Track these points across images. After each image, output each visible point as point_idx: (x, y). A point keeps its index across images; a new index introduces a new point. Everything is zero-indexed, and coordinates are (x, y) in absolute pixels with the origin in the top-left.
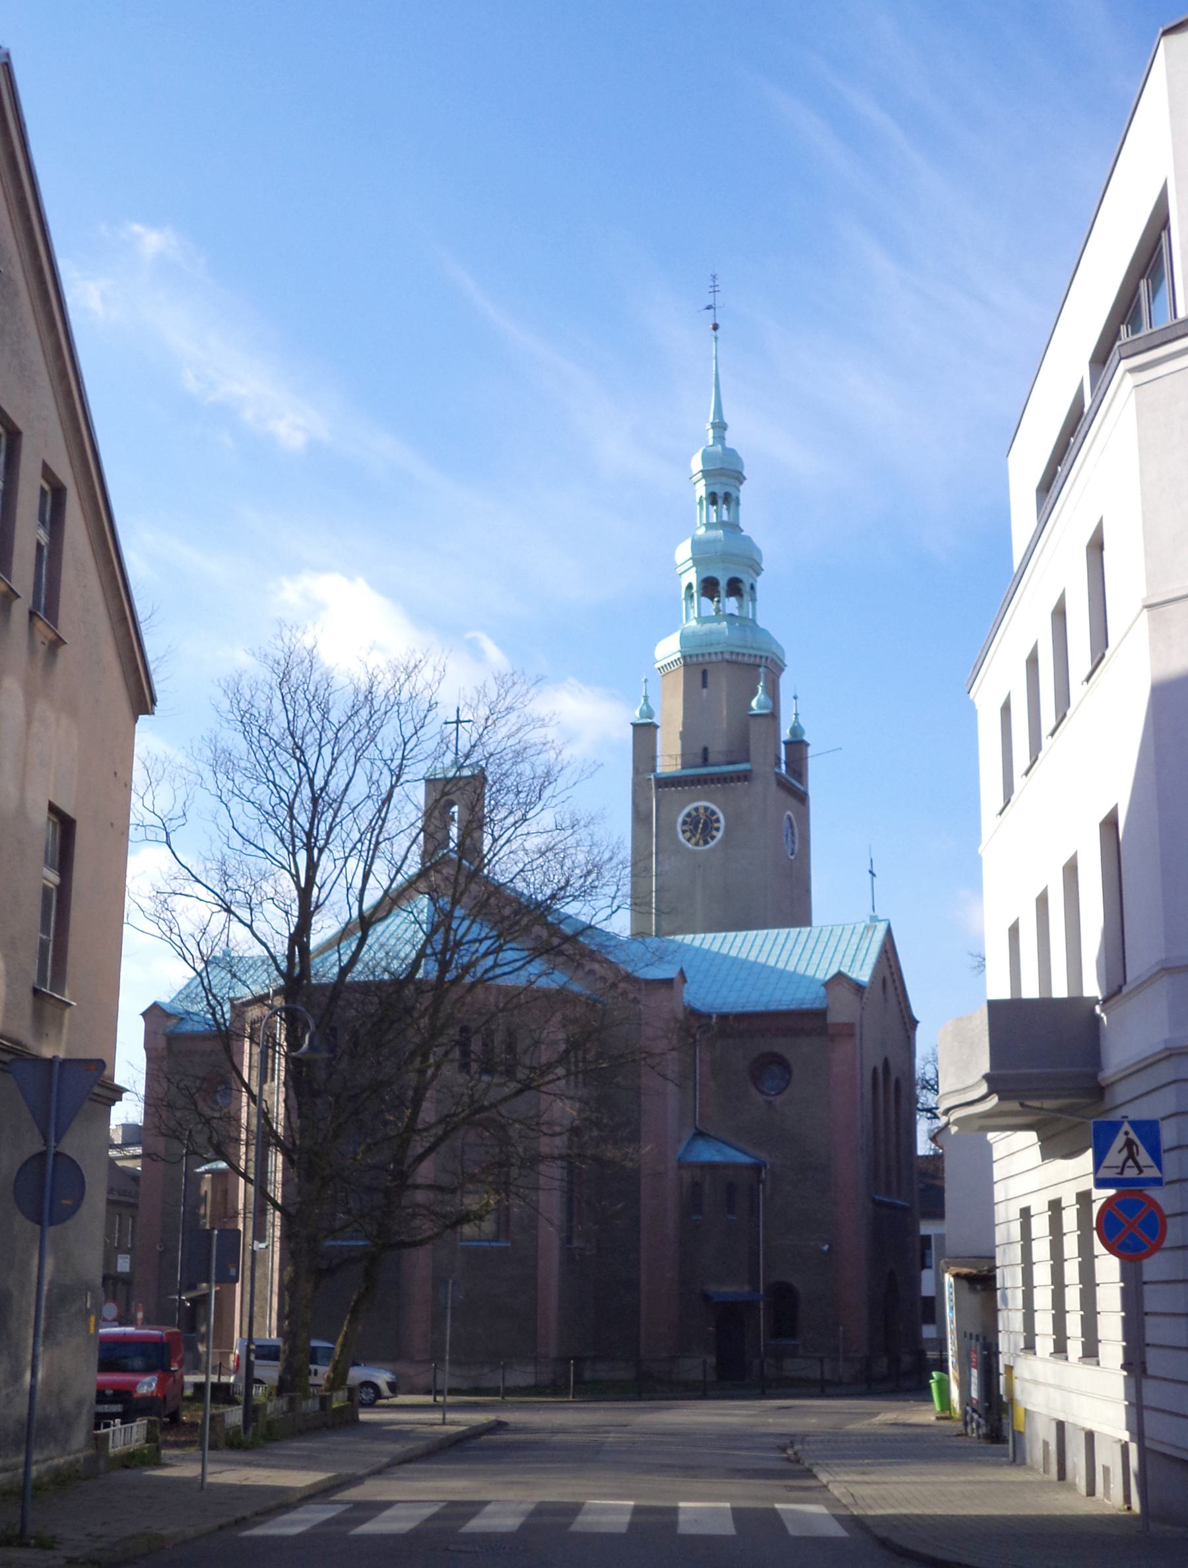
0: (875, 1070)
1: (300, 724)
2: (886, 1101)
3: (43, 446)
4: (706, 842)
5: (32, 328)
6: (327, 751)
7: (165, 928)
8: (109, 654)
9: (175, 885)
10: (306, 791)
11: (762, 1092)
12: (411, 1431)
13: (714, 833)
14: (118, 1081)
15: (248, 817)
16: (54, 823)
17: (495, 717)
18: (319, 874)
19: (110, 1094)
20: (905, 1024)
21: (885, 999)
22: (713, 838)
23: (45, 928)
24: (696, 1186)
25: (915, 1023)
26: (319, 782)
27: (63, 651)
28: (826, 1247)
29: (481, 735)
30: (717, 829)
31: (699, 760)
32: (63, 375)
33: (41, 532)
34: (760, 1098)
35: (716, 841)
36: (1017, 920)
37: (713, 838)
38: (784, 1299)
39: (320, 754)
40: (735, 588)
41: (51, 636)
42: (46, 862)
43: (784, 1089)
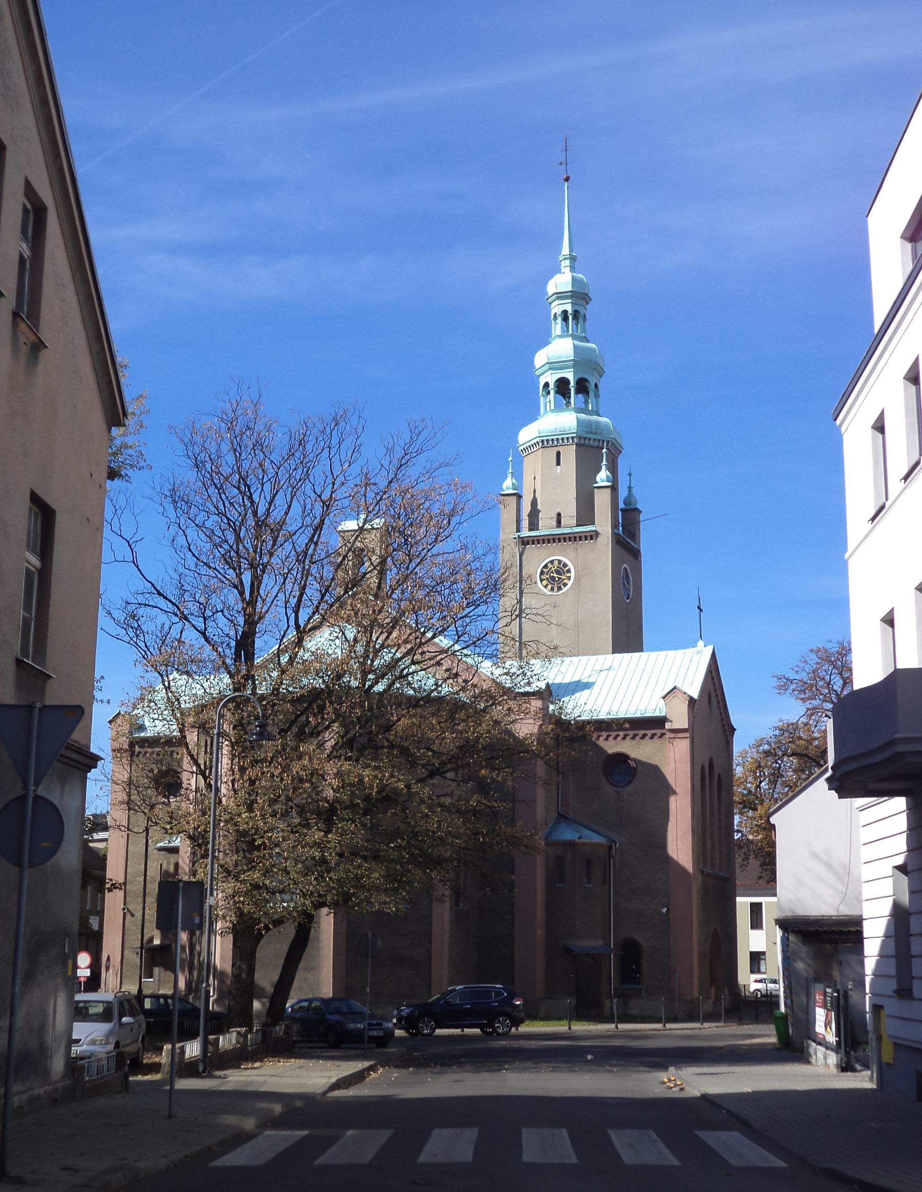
0: (703, 767)
1: (246, 465)
3: (27, 163)
4: (559, 589)
5: (15, 52)
6: (267, 487)
7: (132, 635)
8: (85, 365)
9: (141, 599)
10: (251, 522)
11: (612, 785)
14: (93, 749)
15: (202, 544)
16: (36, 514)
17: (408, 457)
18: (263, 586)
19: (86, 761)
21: (710, 710)
23: (27, 607)
24: (560, 860)
26: (261, 511)
27: (44, 354)
28: (664, 910)
29: (396, 475)
31: (554, 523)
32: (44, 102)
33: (24, 245)
34: (610, 789)
35: (567, 587)
36: (893, 609)
37: (565, 585)
38: (631, 954)
39: (262, 489)
41: (33, 338)
42: (28, 546)
43: (631, 781)
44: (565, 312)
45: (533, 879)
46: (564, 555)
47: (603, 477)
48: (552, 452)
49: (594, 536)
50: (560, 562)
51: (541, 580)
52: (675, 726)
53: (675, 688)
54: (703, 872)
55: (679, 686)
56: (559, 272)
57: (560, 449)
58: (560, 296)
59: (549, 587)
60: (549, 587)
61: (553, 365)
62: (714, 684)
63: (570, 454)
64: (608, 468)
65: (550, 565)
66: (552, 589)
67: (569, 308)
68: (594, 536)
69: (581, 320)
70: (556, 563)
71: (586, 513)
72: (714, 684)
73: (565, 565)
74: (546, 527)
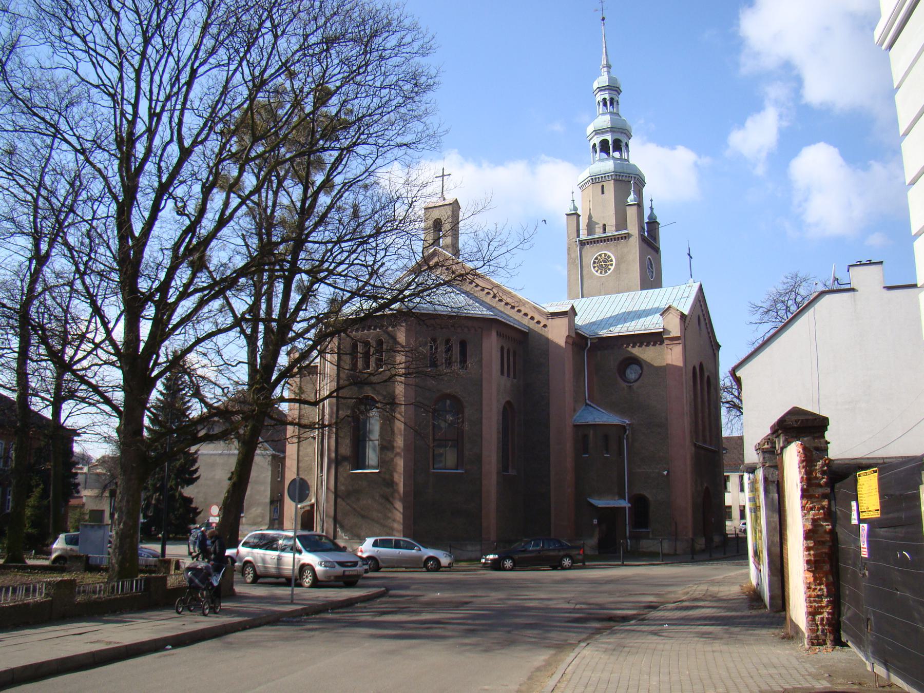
0: (694, 368)
2: (702, 389)
4: (606, 272)
25: (718, 346)
28: (665, 473)
38: (640, 505)
40: (618, 145)
44: (604, 99)
45: (562, 450)
47: (631, 199)
48: (599, 186)
49: (627, 237)
50: (606, 255)
52: (671, 335)
53: (670, 307)
55: (675, 305)
57: (604, 183)
58: (601, 89)
61: (597, 132)
63: (610, 187)
64: (635, 194)
67: (607, 97)
69: (615, 103)
71: (621, 222)
73: (609, 257)
74: (599, 234)
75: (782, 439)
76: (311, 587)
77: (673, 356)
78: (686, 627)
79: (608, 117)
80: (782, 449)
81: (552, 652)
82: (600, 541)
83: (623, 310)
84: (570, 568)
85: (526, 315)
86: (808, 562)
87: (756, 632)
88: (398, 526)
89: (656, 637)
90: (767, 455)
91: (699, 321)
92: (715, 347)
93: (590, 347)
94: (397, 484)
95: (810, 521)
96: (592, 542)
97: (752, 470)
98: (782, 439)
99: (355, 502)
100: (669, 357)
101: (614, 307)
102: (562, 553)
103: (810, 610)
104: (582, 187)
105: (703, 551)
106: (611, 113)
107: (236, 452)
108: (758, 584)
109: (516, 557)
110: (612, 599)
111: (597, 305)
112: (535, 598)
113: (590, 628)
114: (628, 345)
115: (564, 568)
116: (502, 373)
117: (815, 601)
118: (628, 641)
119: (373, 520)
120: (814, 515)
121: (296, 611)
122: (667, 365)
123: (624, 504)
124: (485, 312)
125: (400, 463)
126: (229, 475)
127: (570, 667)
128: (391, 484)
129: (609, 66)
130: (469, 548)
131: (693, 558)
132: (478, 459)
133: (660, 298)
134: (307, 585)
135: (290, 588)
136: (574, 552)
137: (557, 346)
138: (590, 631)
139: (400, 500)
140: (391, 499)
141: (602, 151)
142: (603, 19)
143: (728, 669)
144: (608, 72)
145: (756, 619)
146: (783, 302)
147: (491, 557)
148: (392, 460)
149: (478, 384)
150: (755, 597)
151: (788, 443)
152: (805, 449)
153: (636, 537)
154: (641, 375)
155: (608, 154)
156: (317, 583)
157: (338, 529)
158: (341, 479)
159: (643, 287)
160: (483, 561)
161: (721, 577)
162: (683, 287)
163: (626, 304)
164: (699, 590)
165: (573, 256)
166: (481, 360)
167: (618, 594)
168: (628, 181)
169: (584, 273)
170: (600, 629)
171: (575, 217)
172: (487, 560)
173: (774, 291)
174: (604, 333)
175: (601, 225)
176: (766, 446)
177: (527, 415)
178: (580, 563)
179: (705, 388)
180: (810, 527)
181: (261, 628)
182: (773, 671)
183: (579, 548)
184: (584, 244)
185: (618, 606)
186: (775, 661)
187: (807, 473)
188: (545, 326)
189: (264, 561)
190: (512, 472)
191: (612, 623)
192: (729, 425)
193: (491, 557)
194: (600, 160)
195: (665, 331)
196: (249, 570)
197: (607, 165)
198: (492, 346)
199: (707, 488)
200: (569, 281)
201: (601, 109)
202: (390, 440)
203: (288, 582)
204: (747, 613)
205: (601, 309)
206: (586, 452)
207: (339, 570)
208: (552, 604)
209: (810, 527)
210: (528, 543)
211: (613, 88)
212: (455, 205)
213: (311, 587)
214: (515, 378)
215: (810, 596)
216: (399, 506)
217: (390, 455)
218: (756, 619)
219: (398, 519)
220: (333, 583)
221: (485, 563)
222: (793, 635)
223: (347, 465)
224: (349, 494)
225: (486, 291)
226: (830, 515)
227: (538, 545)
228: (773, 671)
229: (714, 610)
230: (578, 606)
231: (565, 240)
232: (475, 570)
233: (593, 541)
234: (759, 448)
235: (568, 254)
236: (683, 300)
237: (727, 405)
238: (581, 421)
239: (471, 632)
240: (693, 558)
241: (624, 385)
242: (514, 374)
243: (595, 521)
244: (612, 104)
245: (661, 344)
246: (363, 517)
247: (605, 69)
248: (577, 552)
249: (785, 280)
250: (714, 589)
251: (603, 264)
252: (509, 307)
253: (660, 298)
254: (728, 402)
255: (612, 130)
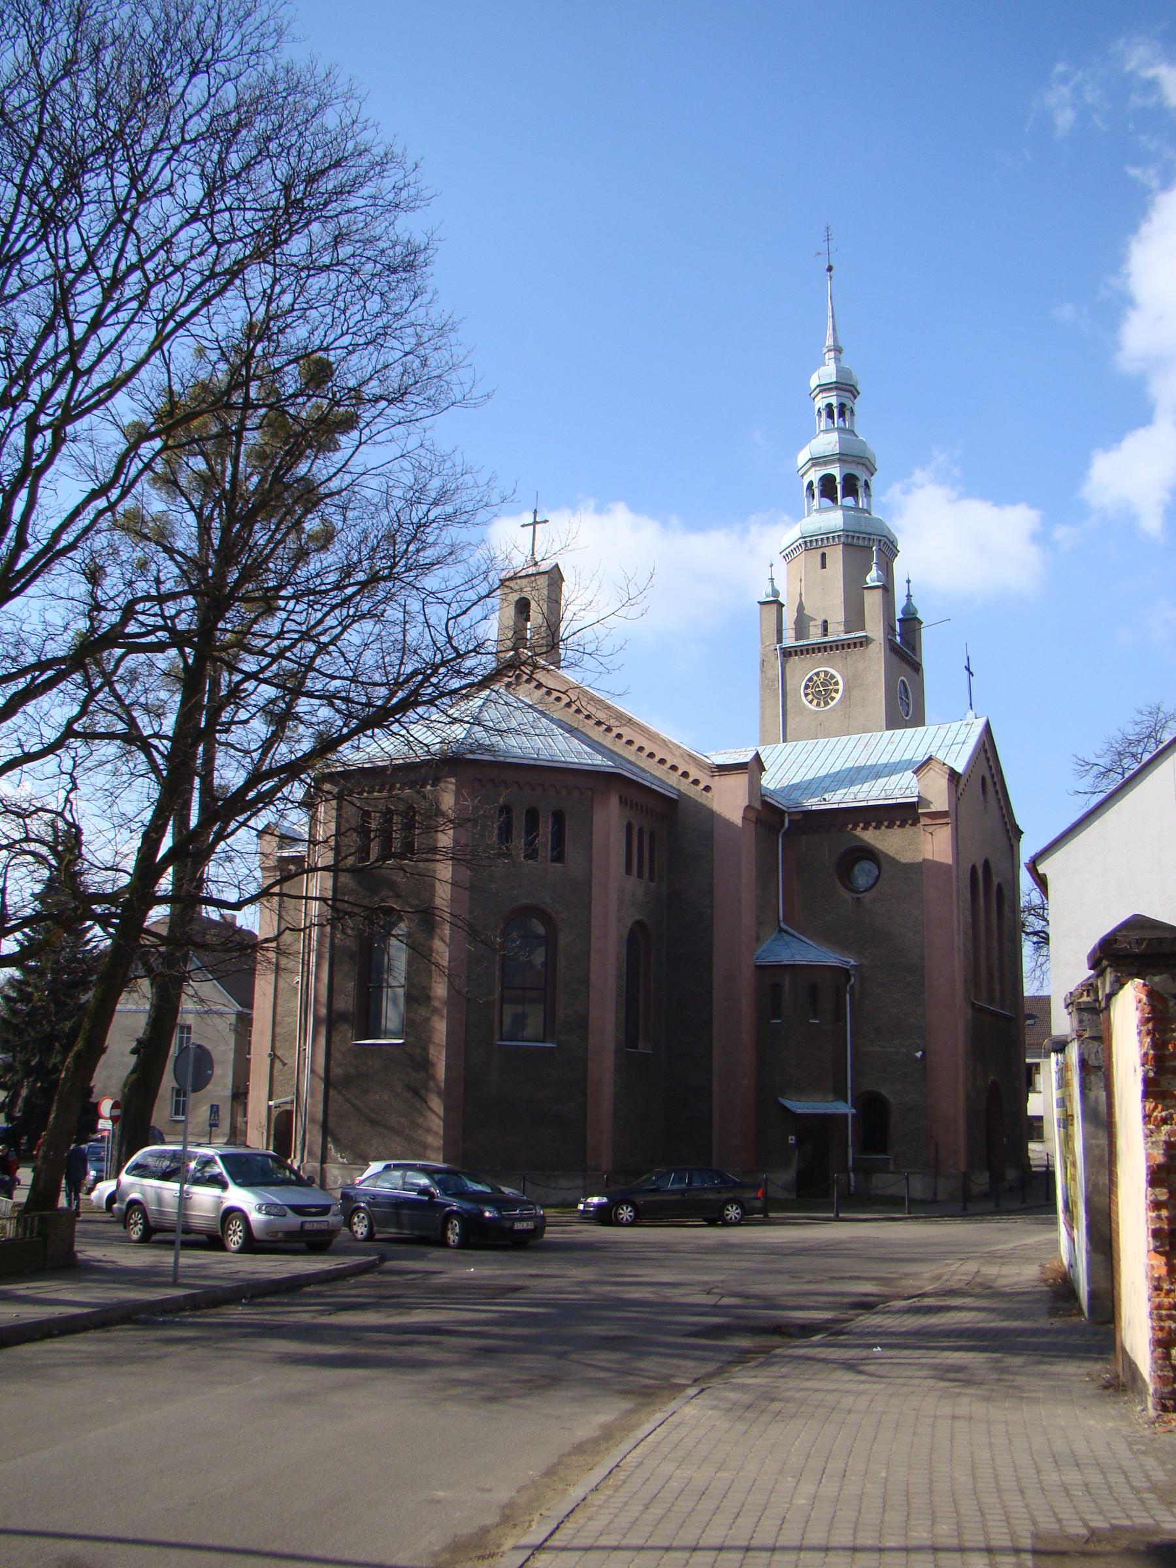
0: (974, 868)
4: (826, 703)
12: (1014, 1248)
13: (834, 694)
20: (1008, 831)
22: (833, 699)
28: (919, 1054)
30: (837, 691)
35: (835, 701)
37: (833, 699)
38: (873, 1109)
40: (851, 486)
44: (829, 406)
46: (833, 669)
47: (873, 577)
49: (864, 642)
50: (826, 673)
51: (806, 695)
52: (933, 809)
53: (930, 758)
54: (973, 1005)
55: (940, 756)
56: (824, 365)
57: (825, 550)
58: (824, 388)
59: (815, 702)
60: (815, 702)
61: (816, 461)
62: (990, 767)
63: (836, 556)
64: (879, 568)
65: (815, 678)
66: (818, 705)
67: (834, 401)
68: (864, 642)
69: (848, 413)
70: (822, 675)
71: (855, 618)
72: (990, 767)
73: (832, 677)
74: (815, 636)
75: (1109, 977)
76: (241, 1251)
77: (935, 846)
78: (918, 1353)
79: (834, 437)
80: (1109, 997)
81: (627, 1405)
82: (800, 1173)
83: (849, 765)
84: (737, 1224)
85: (674, 768)
86: (1156, 1234)
87: (1056, 1368)
88: (435, 1141)
89: (849, 1376)
90: (1086, 1016)
91: (983, 783)
92: (1014, 833)
93: (791, 830)
94: (433, 1065)
95: (1162, 1146)
96: (782, 1178)
97: (1060, 1047)
98: (1109, 977)
99: (358, 1099)
100: (929, 847)
101: (832, 759)
102: (725, 1196)
103: (1160, 1335)
104: (788, 556)
105: (985, 1196)
106: (841, 430)
107: (148, 1007)
108: (1071, 1266)
109: (640, 1200)
110: (791, 1288)
111: (803, 756)
112: (648, 1282)
113: (728, 1348)
114: (855, 826)
115: (727, 1224)
116: (628, 870)
117: (1170, 1317)
118: (792, 1383)
119: (391, 1129)
120: (1169, 1134)
121: (74, 1317)
122: (924, 860)
123: (845, 1108)
124: (598, 760)
125: (440, 1028)
126: (134, 1044)
127: (638, 1450)
128: (424, 1064)
129: (838, 350)
130: (563, 1183)
131: (965, 1209)
132: (582, 1023)
133: (914, 745)
134: (233, 1247)
135: (172, 1253)
136: (748, 1194)
137: (729, 824)
138: (726, 1357)
139: (439, 1094)
140: (423, 1092)
141: (823, 494)
142: (830, 269)
143: (973, 1466)
144: (837, 360)
145: (1061, 1339)
146: (1133, 755)
147: (595, 1200)
148: (429, 1019)
149: (583, 891)
150: (1062, 1289)
151: (1119, 984)
152: (1151, 994)
153: (865, 1170)
154: (878, 877)
155: (834, 499)
156: (252, 1245)
157: (330, 1146)
158: (336, 1055)
159: (888, 729)
160: (581, 1207)
161: (1011, 1246)
162: (956, 726)
163: (855, 754)
164: (959, 1271)
165: (770, 674)
166: (590, 848)
167: (810, 1277)
168: (868, 548)
169: (789, 704)
170: (746, 1351)
171: (775, 606)
172: (587, 1205)
173: (1119, 736)
174: (813, 803)
175: (819, 622)
176: (1085, 999)
177: (671, 947)
178: (758, 1212)
179: (993, 899)
180: (1160, 1159)
181: (89, 1335)
182: (1072, 1476)
183: (755, 1186)
184: (790, 654)
185: (802, 1301)
186: (1080, 1446)
187: (1155, 1045)
188: (707, 789)
189: (160, 1200)
190: (643, 1048)
191: (777, 1340)
192: (1038, 973)
193: (595, 1200)
194: (821, 510)
195: (922, 801)
196: (136, 1217)
197: (833, 519)
198: (609, 821)
199: (994, 1082)
200: (762, 717)
201: (823, 422)
202: (425, 990)
203: (214, 1241)
204: (1044, 1322)
205: (809, 762)
206: (777, 1015)
207: (293, 1221)
208: (676, 1295)
209: (1160, 1159)
210: (663, 1176)
211: (845, 387)
212: (555, 577)
213: (241, 1251)
214: (651, 879)
215: (1159, 1307)
216: (436, 1104)
217: (423, 1012)
218: (1061, 1339)
219: (435, 1128)
220: (283, 1245)
221: (584, 1212)
222: (1123, 1383)
223: (346, 1030)
224: (348, 1080)
225: (555, 694)
226: (1064, 1093)
227: (681, 1180)
228: (1072, 1476)
229: (982, 1315)
230: (727, 1301)
231: (758, 647)
232: (567, 1223)
233: (786, 1176)
234: (1072, 1003)
235: (762, 671)
236: (956, 748)
237: (1035, 939)
238: (770, 960)
239: (487, 1353)
240: (965, 1209)
241: (847, 895)
242: (652, 870)
243: (792, 1139)
244: (842, 414)
245: (914, 824)
246: (374, 1123)
247: (832, 354)
248: (752, 1195)
249: (1138, 718)
250: (991, 1270)
251: (821, 690)
252: (592, 722)
253: (914, 745)
254: (1035, 933)
255: (842, 458)
